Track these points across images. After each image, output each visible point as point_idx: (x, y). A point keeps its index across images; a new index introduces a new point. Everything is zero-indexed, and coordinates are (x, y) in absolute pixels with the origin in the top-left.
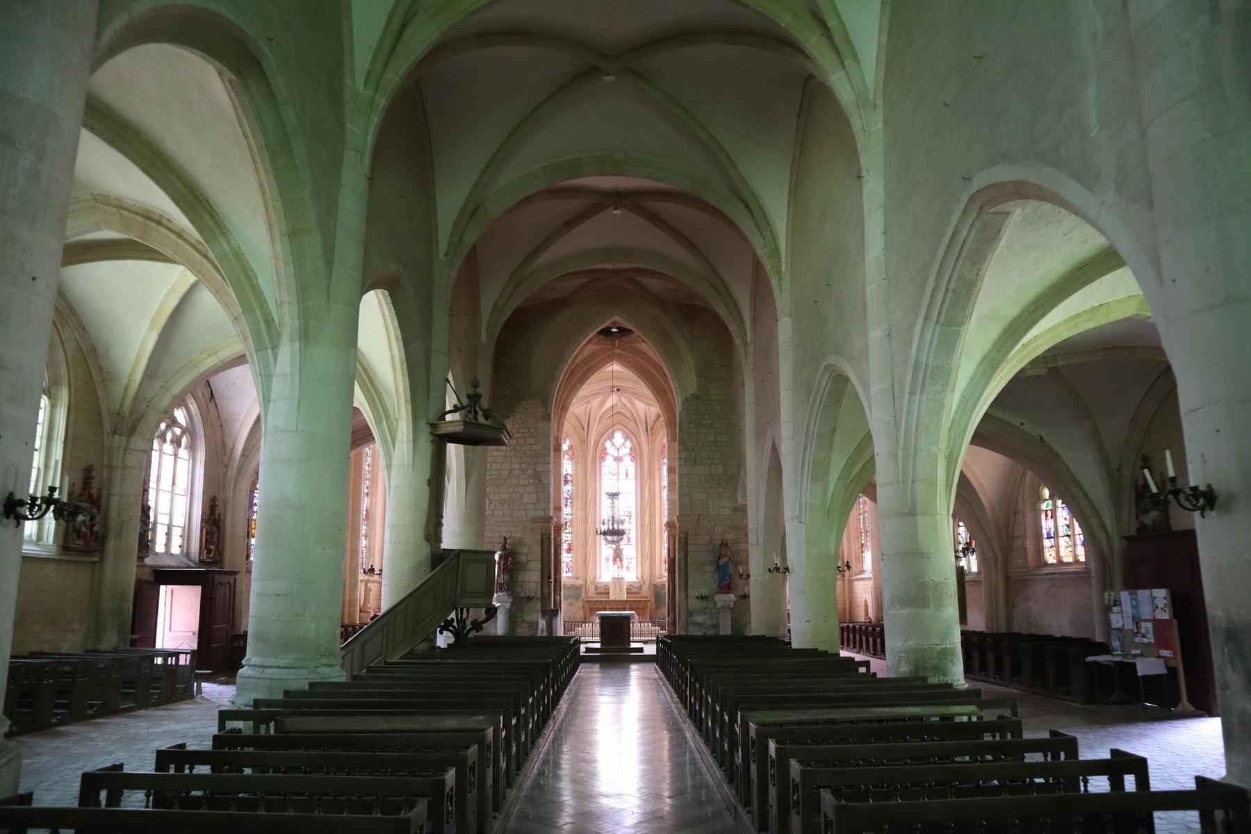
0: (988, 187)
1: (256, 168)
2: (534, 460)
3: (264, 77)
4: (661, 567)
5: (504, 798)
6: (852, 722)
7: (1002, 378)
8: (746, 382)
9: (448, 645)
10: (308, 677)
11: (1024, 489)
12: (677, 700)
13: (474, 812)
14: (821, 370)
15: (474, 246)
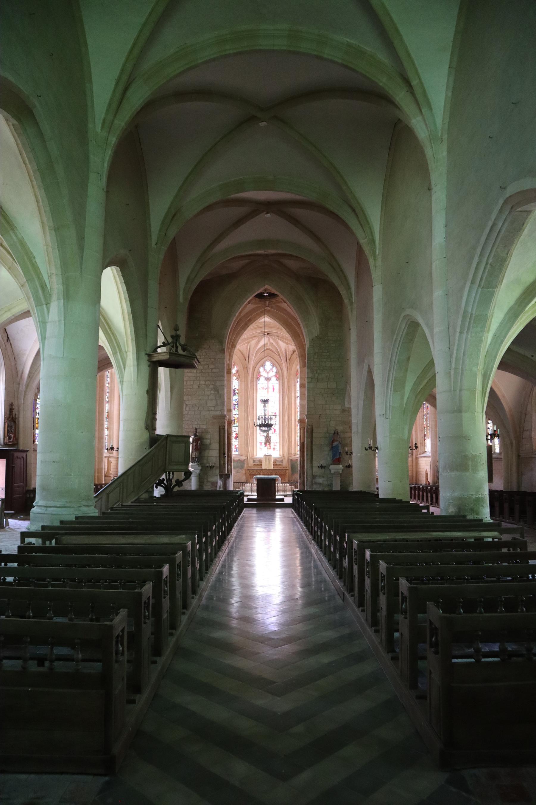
0: (518, 193)
1: (32, 185)
2: (215, 379)
3: (36, 123)
4: (295, 448)
5: (198, 586)
6: (418, 541)
7: (521, 324)
8: (351, 327)
9: (161, 495)
10: (75, 513)
11: (532, 398)
12: (306, 530)
13: (180, 592)
14: (400, 320)
15: (174, 238)
